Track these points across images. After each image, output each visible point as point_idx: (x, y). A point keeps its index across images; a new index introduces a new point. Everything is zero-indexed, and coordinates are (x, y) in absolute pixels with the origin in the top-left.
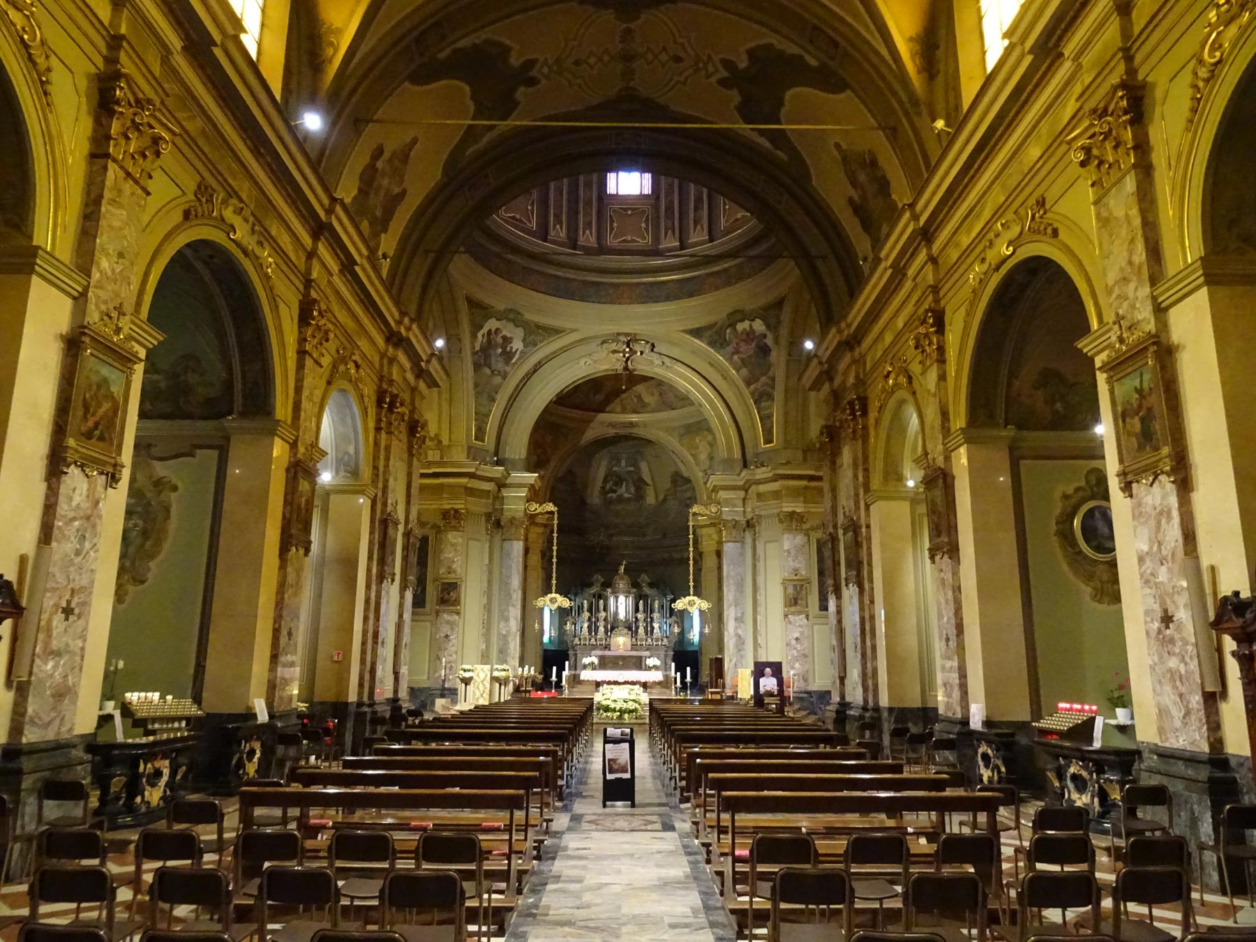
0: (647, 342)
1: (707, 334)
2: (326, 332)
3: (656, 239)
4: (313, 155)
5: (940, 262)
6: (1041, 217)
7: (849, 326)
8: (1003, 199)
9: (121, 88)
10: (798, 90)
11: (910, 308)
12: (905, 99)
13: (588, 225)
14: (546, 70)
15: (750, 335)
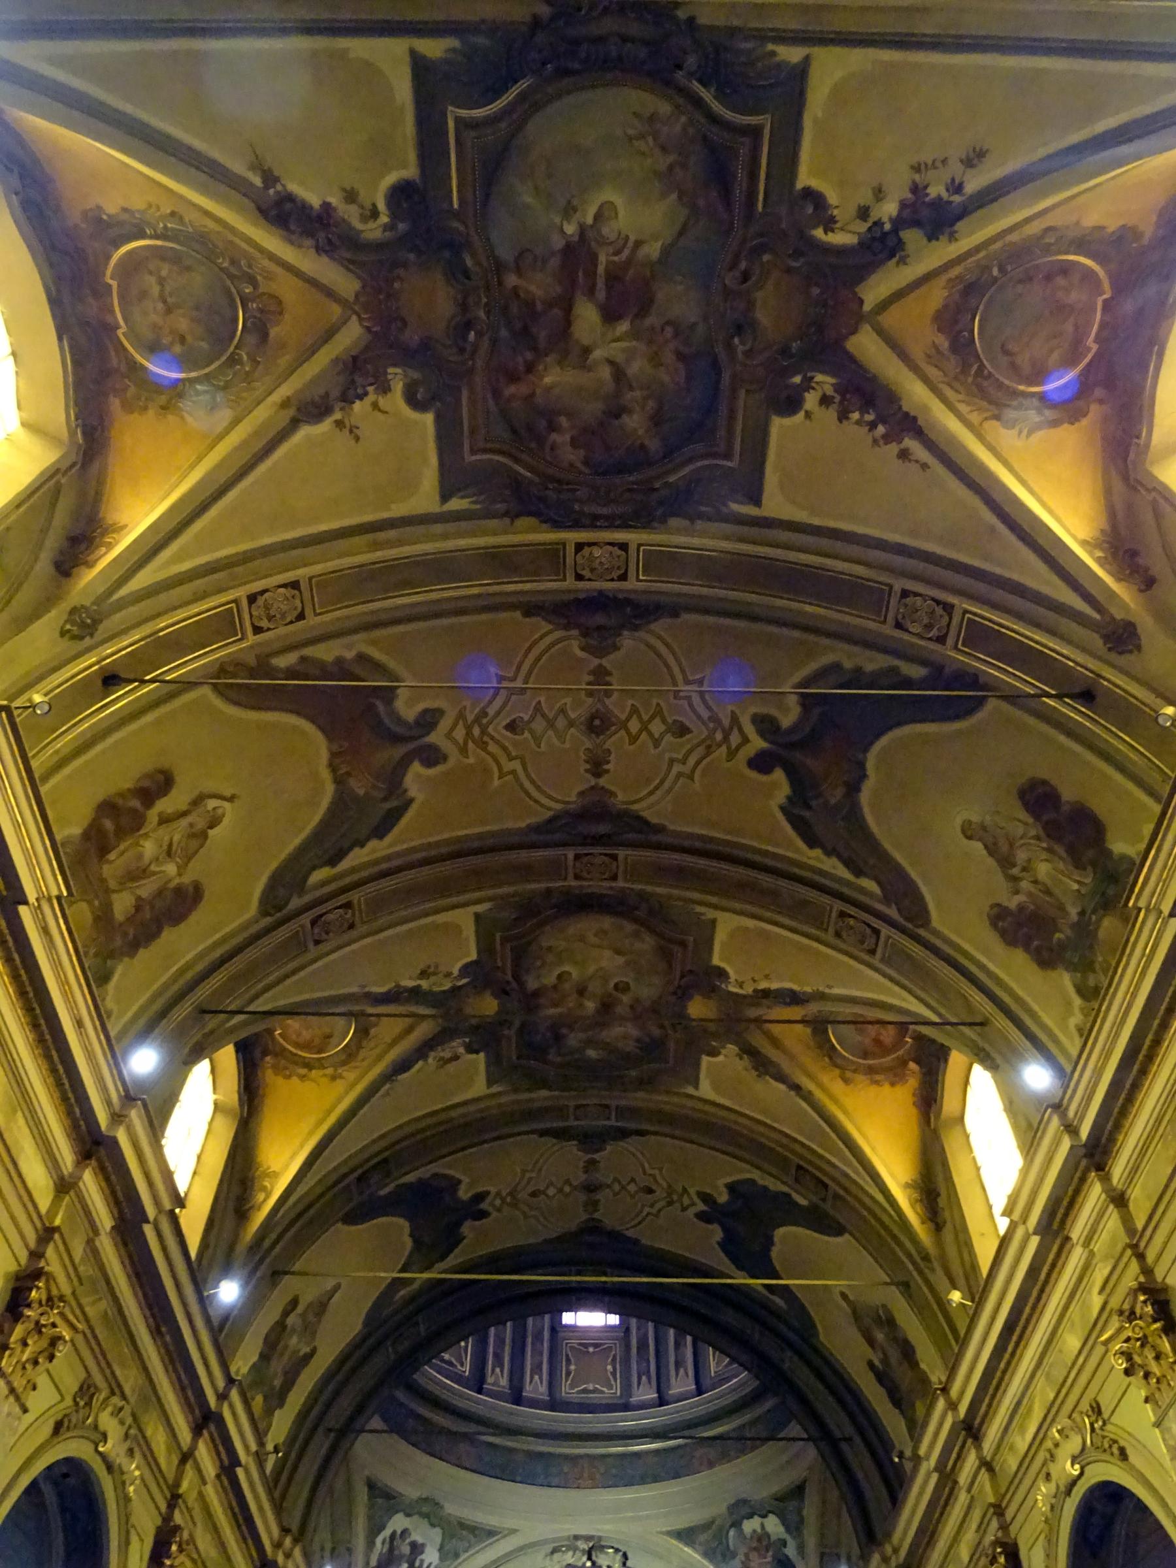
0: (617, 1550)
1: (703, 1538)
2: (54, 1341)
3: (627, 1388)
4: (216, 1323)
5: (997, 1469)
6: (1102, 1429)
7: (896, 1551)
8: (1052, 1396)
9: (38, 1288)
10: (793, 1229)
11: (970, 1536)
12: (913, 1251)
13: (537, 1369)
14: (498, 1202)
15: (762, 1541)
